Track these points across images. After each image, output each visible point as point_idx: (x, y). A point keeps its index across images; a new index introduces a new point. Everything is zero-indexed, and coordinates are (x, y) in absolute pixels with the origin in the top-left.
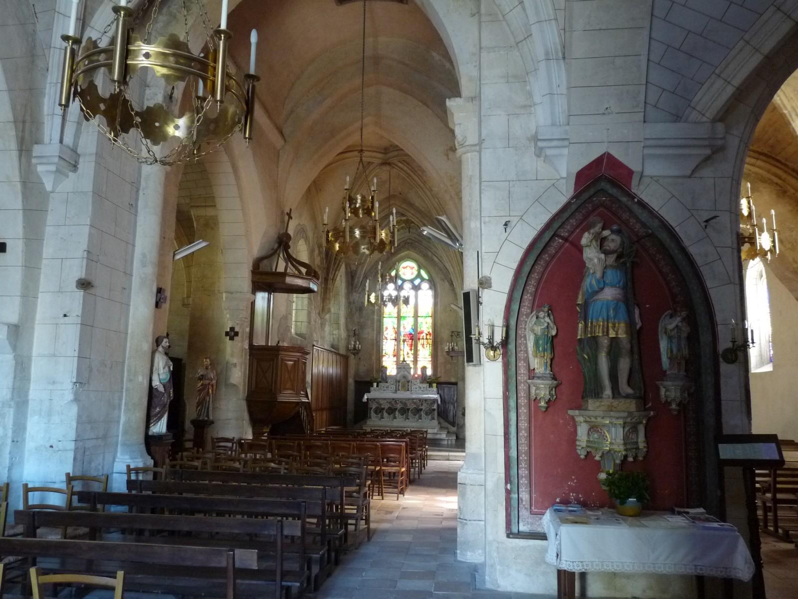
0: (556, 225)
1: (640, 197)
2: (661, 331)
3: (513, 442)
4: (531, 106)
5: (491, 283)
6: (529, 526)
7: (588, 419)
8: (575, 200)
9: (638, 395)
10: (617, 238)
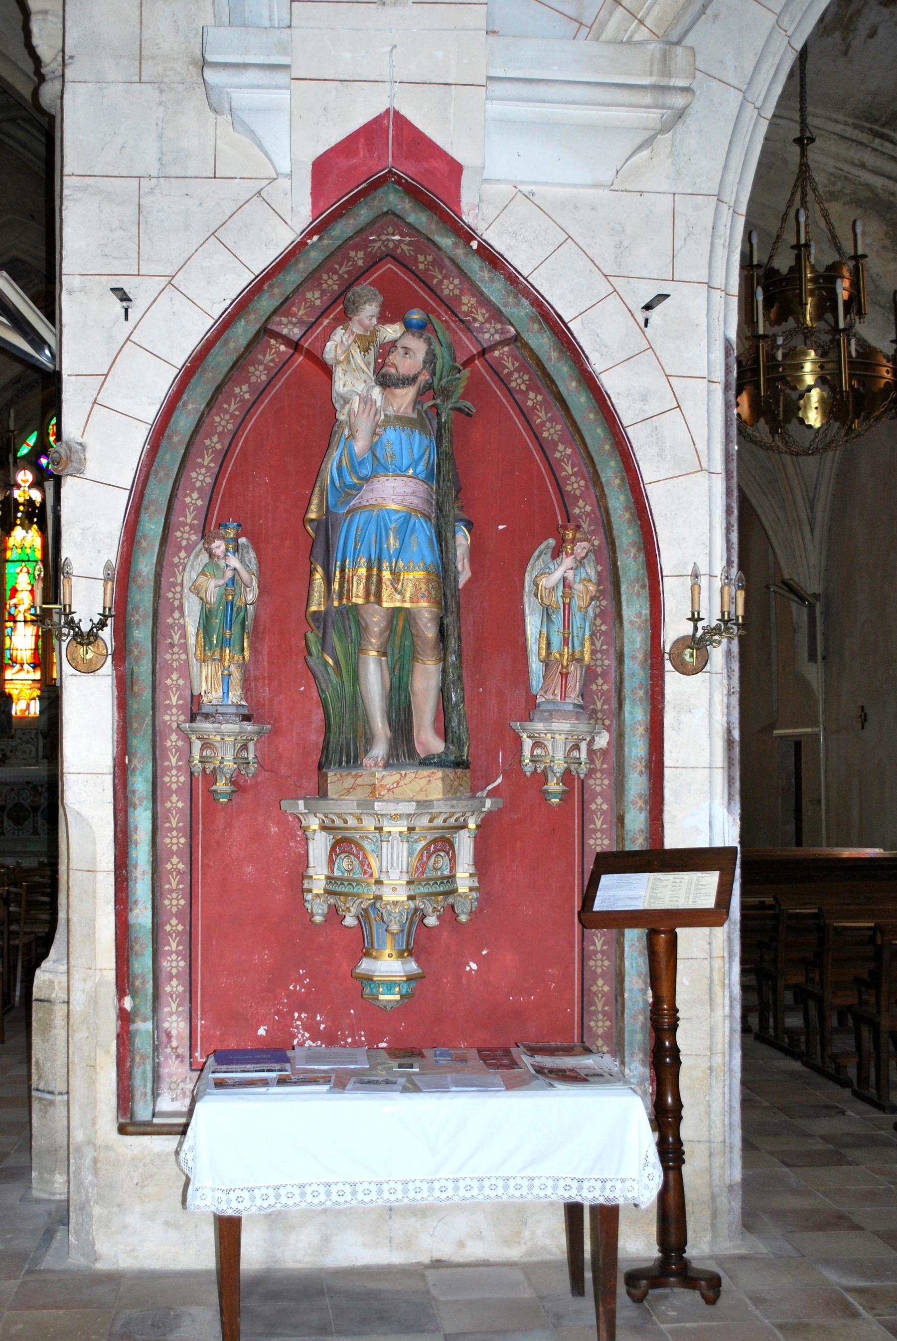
0: (266, 303)
1: (485, 237)
3: (142, 888)
8: (315, 238)
9: (452, 758)
10: (418, 347)
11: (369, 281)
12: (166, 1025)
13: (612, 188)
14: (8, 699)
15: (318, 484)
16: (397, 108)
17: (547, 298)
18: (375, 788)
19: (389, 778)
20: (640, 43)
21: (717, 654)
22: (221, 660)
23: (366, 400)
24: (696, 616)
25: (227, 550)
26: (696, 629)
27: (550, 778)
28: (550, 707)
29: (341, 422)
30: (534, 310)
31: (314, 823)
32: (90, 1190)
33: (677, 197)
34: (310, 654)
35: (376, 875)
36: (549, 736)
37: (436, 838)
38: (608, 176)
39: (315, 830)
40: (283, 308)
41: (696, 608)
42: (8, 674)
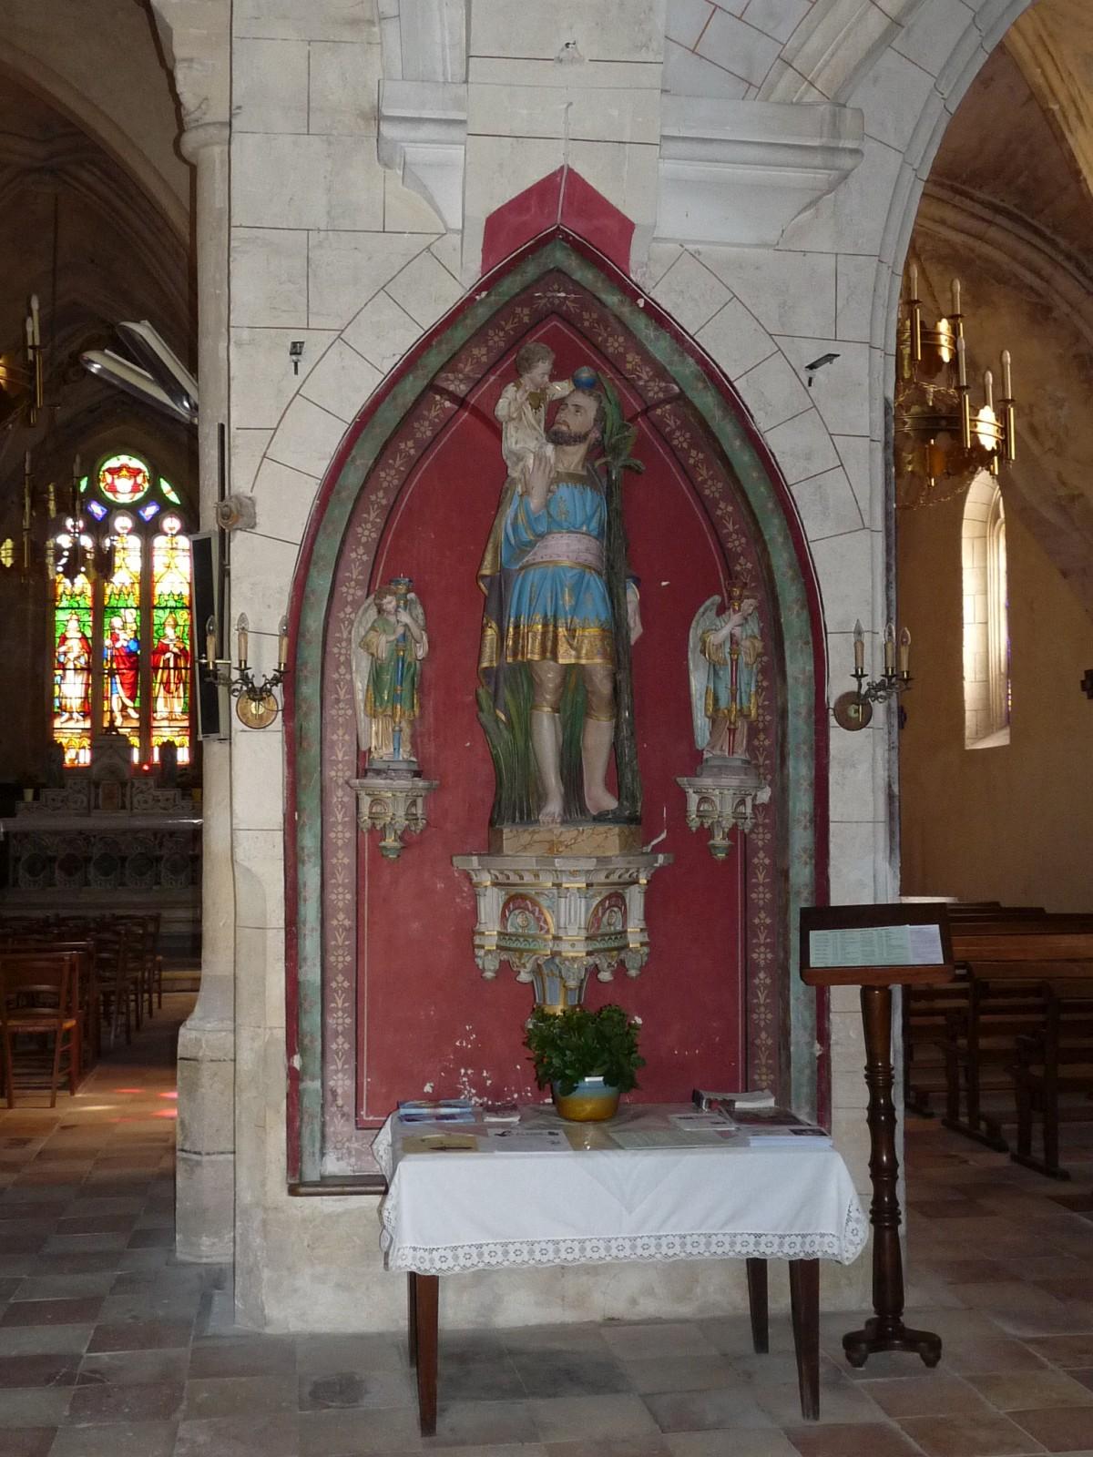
0: (434, 360)
1: (652, 295)
2: (695, 647)
3: (310, 945)
4: (371, 23)
5: (254, 516)
6: (353, 1160)
7: (502, 879)
8: (484, 294)
10: (589, 404)
11: (535, 338)
12: (331, 1083)
13: (777, 248)
14: (60, 749)
15: (491, 540)
16: (571, 166)
17: (713, 357)
18: (553, 845)
19: (568, 834)
20: (810, 105)
21: (879, 709)
22: (393, 716)
23: (540, 458)
24: (860, 673)
25: (398, 606)
26: (860, 686)
27: (716, 833)
28: (716, 763)
29: (513, 479)
30: (699, 368)
31: (486, 879)
32: (259, 1254)
33: (839, 257)
34: (481, 710)
35: (553, 931)
36: (717, 792)
37: (611, 894)
38: (772, 236)
39: (486, 887)
40: (450, 365)
41: (860, 665)
42: (57, 723)
